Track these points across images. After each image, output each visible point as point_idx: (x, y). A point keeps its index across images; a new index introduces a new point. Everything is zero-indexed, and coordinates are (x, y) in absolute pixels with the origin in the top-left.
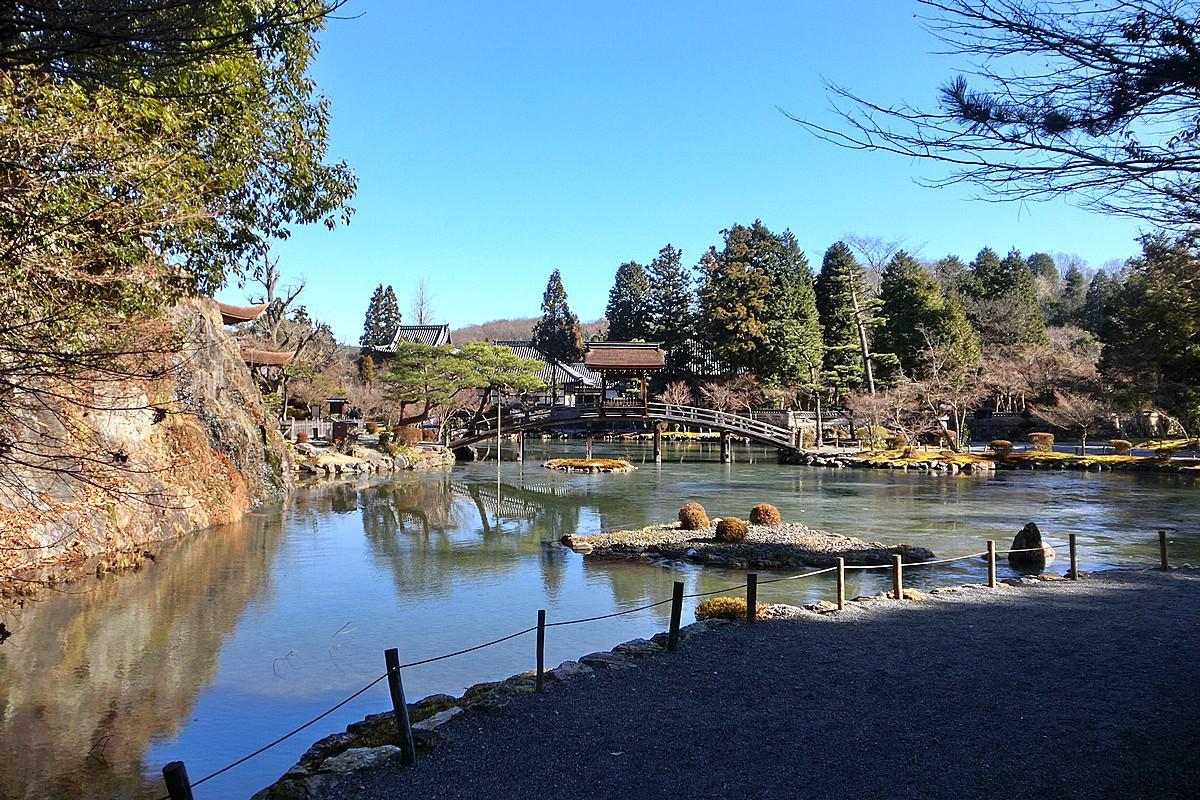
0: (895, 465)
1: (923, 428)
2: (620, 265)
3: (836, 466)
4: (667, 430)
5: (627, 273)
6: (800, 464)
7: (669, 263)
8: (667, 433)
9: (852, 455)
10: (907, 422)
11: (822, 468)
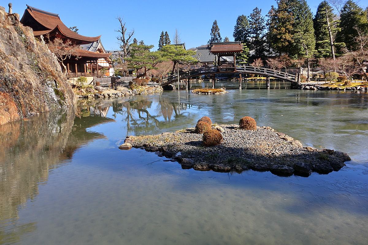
0: (340, 88)
1: (355, 72)
2: (238, 17)
3: (314, 89)
4: (255, 77)
5: (241, 19)
6: (298, 89)
7: (256, 15)
8: (254, 78)
9: (322, 85)
10: (347, 71)
11: (308, 91)
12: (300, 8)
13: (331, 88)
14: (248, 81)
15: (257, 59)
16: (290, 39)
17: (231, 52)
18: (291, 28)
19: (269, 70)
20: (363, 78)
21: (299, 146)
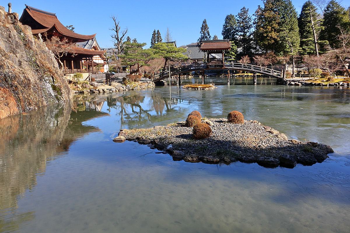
0: (324, 84)
1: (337, 68)
2: (226, 16)
3: (298, 85)
4: (242, 73)
5: (229, 19)
6: (284, 85)
7: (244, 14)
8: (242, 74)
9: (306, 80)
10: (330, 67)
11: (293, 86)
12: (286, 8)
13: (315, 84)
14: (236, 77)
15: (244, 56)
16: (276, 37)
17: (220, 49)
18: (277, 26)
19: (256, 67)
20: (345, 74)
21: (284, 139)
